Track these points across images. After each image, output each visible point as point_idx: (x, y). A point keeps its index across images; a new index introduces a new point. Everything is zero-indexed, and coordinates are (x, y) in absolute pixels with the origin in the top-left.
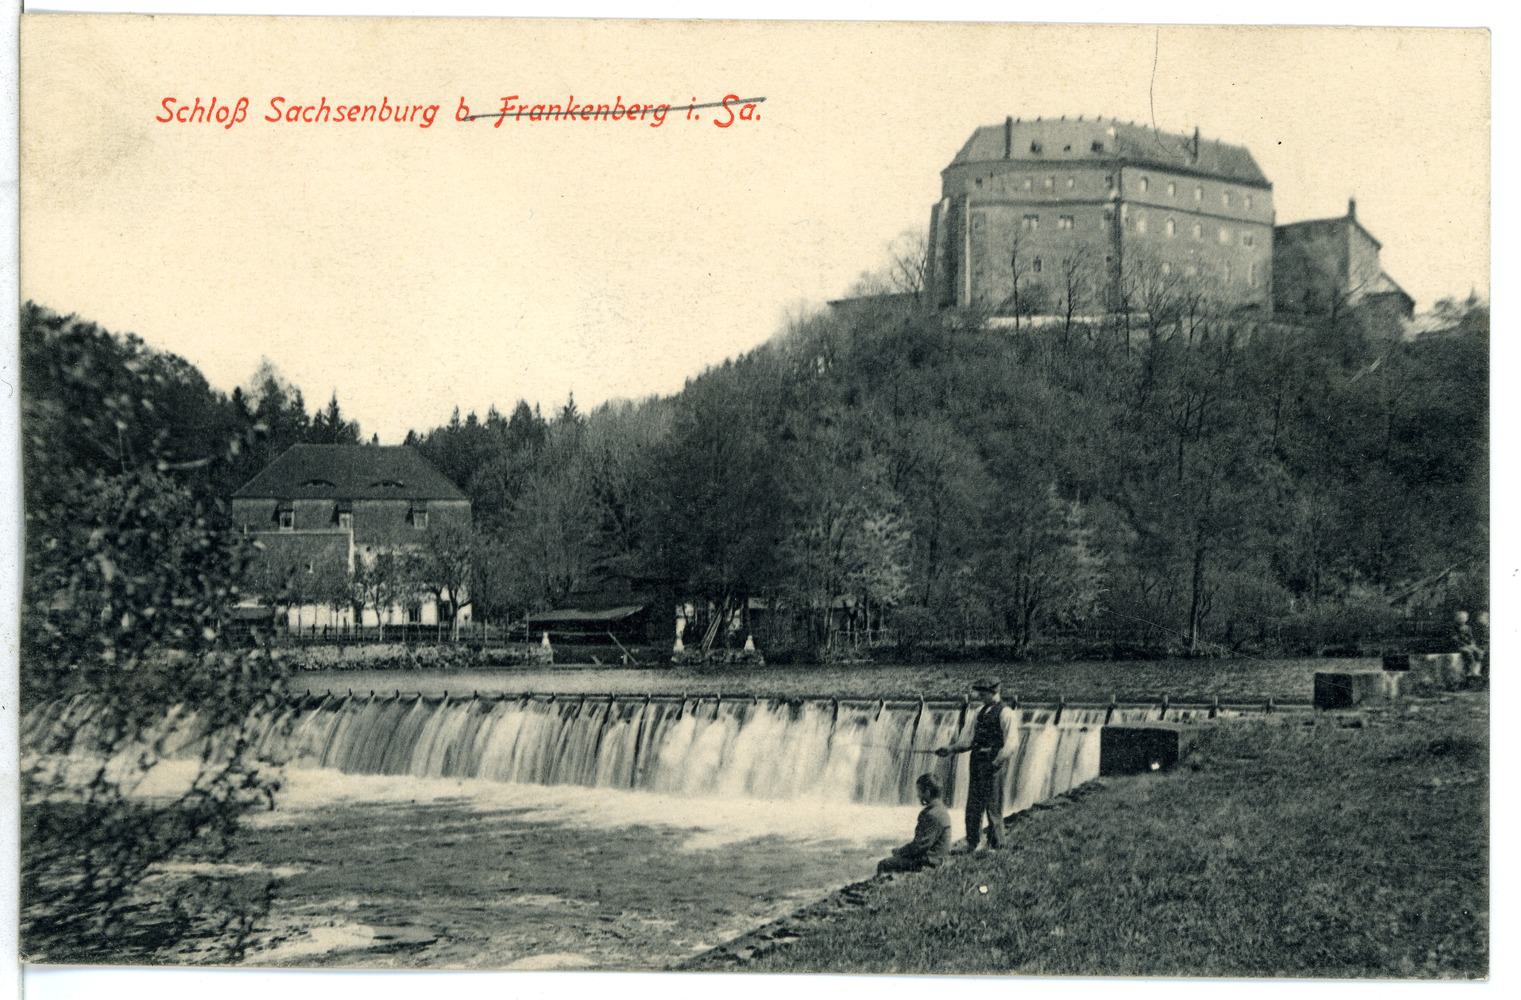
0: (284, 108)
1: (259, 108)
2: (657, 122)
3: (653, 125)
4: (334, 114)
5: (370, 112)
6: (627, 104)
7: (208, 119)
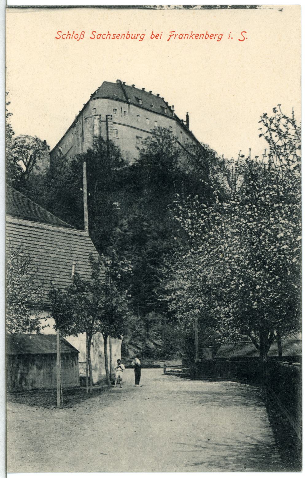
0: (96, 34)
1: (88, 35)
2: (141, 40)
3: (218, 41)
4: (112, 36)
5: (187, 36)
6: (155, 34)
7: (72, 38)
